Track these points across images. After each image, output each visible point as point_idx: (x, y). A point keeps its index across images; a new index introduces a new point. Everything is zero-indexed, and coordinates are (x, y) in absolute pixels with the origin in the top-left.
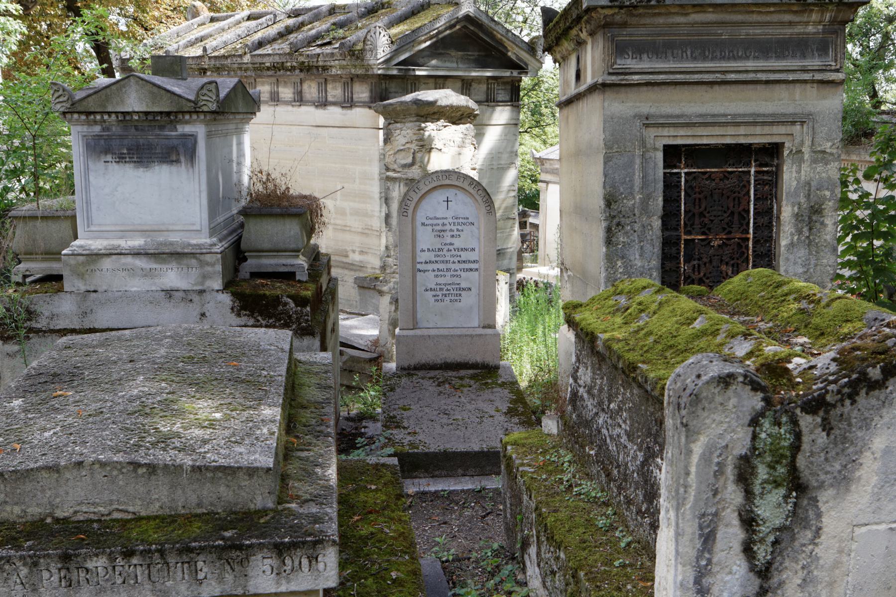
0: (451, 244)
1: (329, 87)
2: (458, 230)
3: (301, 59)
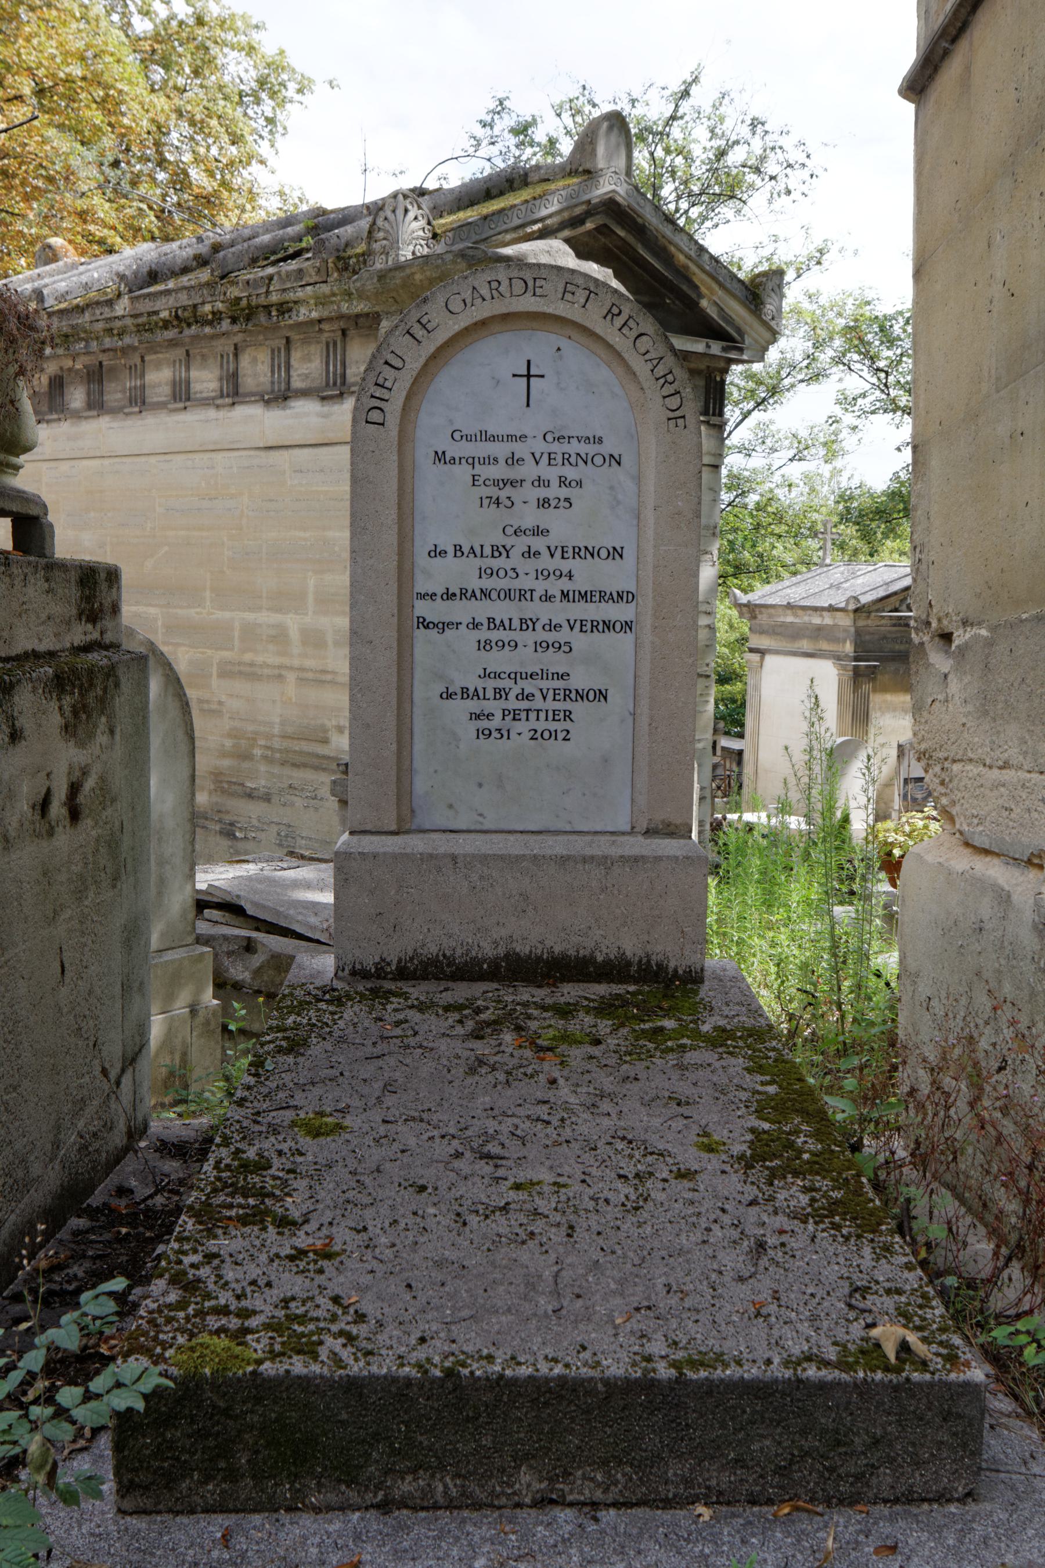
0: (539, 532)
1: (296, 355)
2: (563, 481)
3: (234, 292)
